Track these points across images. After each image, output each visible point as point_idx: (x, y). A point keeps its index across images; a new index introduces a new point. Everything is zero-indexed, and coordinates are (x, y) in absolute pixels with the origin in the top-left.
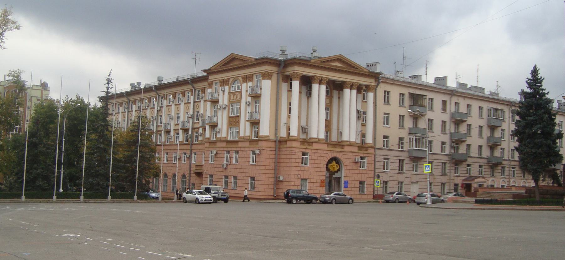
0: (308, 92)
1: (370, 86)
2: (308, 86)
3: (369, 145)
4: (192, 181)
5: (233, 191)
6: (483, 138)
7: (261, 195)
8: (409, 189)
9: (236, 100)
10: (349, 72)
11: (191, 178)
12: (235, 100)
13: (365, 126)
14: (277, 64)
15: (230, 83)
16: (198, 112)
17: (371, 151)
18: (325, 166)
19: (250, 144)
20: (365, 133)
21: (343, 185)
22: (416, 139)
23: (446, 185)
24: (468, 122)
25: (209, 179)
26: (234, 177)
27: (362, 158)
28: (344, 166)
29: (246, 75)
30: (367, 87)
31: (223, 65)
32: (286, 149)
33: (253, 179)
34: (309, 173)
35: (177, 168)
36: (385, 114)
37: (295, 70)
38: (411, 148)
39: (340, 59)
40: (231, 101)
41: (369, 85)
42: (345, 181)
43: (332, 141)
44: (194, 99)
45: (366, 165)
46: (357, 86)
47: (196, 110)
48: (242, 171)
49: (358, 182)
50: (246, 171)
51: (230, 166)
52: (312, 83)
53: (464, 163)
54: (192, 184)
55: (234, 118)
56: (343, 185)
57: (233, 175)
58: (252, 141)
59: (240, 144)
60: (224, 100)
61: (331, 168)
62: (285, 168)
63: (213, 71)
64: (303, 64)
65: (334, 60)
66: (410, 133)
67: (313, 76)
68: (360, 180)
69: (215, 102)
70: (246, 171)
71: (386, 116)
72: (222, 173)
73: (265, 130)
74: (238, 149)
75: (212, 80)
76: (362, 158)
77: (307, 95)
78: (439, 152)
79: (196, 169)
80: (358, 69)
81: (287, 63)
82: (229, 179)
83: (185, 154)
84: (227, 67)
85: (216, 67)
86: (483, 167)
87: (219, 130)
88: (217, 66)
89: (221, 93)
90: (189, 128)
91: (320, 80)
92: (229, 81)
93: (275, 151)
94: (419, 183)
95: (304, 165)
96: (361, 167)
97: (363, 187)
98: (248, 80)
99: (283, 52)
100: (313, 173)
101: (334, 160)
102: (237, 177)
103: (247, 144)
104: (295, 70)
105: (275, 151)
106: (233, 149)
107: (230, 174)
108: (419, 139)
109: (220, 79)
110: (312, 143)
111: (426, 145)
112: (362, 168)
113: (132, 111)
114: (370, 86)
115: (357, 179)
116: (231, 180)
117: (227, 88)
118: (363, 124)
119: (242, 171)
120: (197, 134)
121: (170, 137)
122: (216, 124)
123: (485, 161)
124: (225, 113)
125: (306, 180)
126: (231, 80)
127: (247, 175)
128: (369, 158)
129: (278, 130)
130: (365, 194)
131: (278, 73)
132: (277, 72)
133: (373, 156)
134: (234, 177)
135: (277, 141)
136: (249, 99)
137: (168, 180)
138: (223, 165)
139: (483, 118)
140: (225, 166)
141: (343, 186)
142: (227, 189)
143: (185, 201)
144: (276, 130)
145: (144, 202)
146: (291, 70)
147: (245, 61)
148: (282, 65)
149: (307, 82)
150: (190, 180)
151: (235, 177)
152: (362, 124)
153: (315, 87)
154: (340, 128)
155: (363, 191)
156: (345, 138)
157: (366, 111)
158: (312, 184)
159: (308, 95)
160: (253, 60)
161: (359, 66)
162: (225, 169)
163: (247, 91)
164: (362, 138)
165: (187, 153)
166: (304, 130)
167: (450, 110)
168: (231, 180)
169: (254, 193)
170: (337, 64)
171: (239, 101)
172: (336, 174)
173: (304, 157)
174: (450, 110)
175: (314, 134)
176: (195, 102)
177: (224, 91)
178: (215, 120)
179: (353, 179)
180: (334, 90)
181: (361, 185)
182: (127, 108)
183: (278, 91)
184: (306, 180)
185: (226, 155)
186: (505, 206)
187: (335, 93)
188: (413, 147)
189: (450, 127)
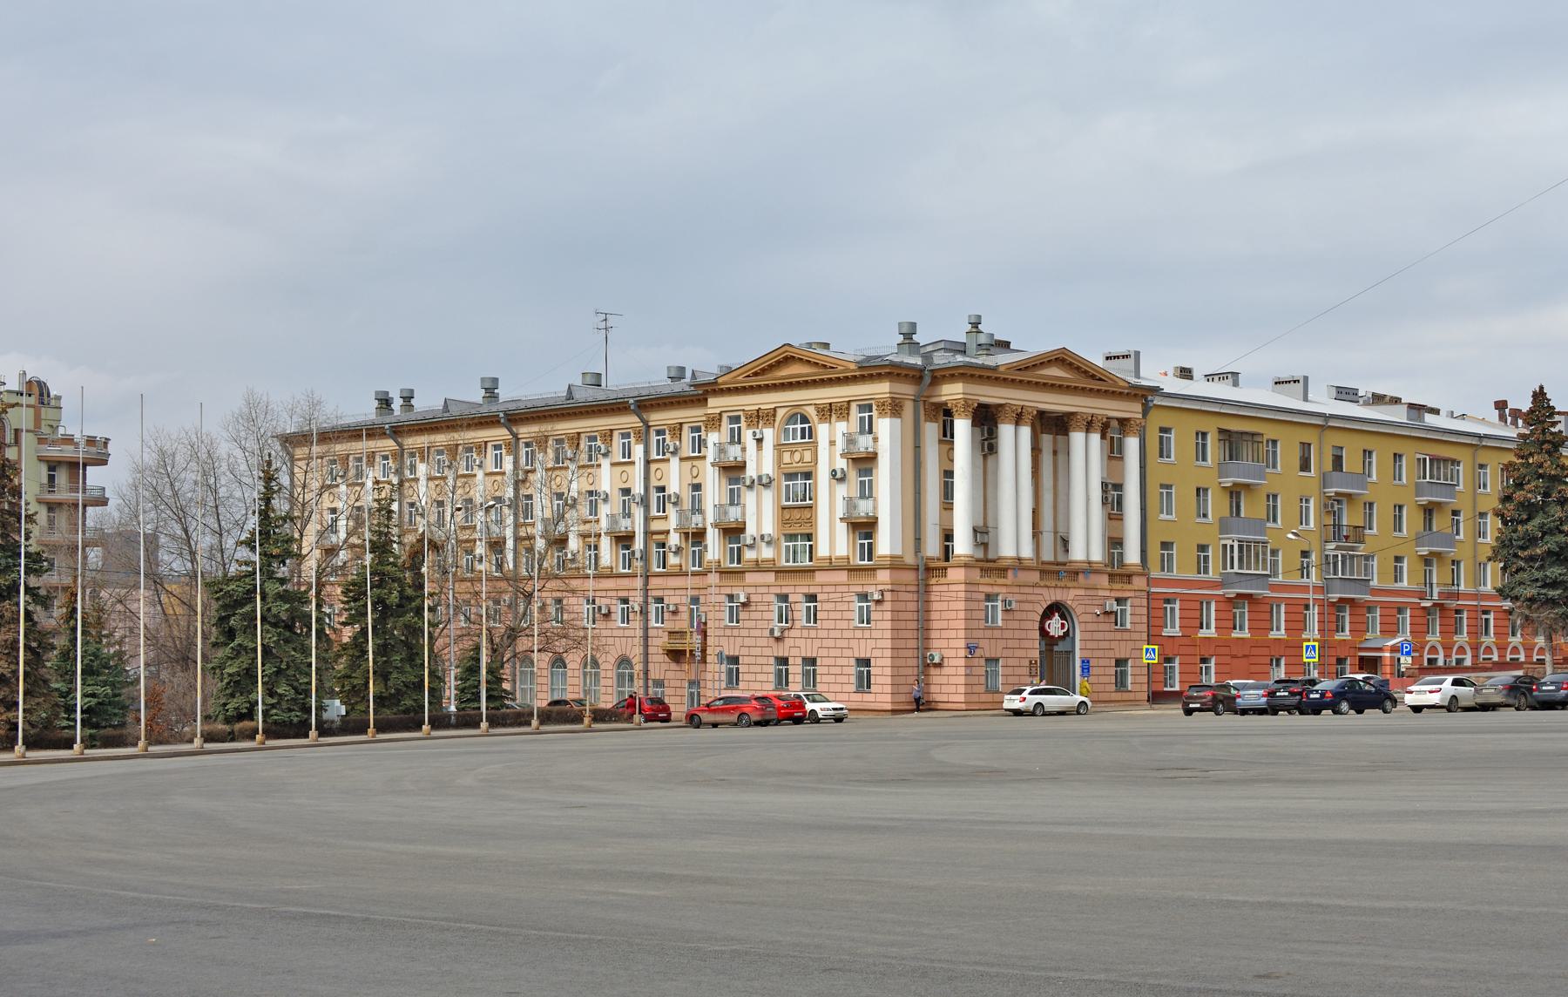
0: (986, 443)
1: (1132, 422)
2: (986, 428)
3: (1133, 569)
4: (654, 674)
8: (1218, 671)
10: (1083, 389)
11: (651, 666)
12: (798, 465)
13: (1122, 520)
14: (913, 376)
15: (778, 419)
16: (662, 489)
17: (1139, 582)
18: (1037, 626)
20: (1122, 539)
22: (1240, 547)
26: (777, 658)
27: (1119, 601)
28: (1080, 623)
29: (830, 404)
30: (1123, 422)
31: (756, 374)
32: (945, 588)
36: (1162, 486)
38: (1229, 570)
39: (1062, 358)
40: (782, 466)
41: (1127, 420)
42: (1083, 662)
43: (1043, 563)
44: (647, 452)
45: (1128, 618)
46: (1102, 424)
47: (654, 483)
49: (1113, 663)
51: (793, 633)
52: (999, 421)
54: (654, 680)
55: (796, 510)
57: (776, 655)
58: (853, 570)
59: (820, 577)
60: (761, 461)
62: (945, 634)
63: (722, 387)
64: (980, 377)
65: (1049, 361)
67: (1001, 405)
68: (1118, 656)
69: (733, 471)
70: (844, 643)
71: (1164, 491)
72: (767, 652)
73: (963, 545)
74: (812, 590)
75: (718, 411)
76: (1119, 601)
77: (983, 450)
79: (671, 641)
81: (938, 374)
82: (739, 666)
83: (625, 601)
85: (735, 377)
87: (752, 542)
88: (739, 376)
89: (751, 444)
90: (634, 532)
91: (1017, 414)
92: (774, 415)
96: (1116, 625)
97: (1124, 674)
98: (834, 417)
99: (908, 334)
100: (826, 643)
101: (1055, 609)
103: (842, 576)
106: (799, 589)
107: (794, 652)
108: (1249, 547)
111: (1264, 560)
112: (1118, 627)
113: (416, 480)
114: (1132, 422)
115: (1111, 654)
116: (796, 669)
117: (769, 434)
118: (1112, 517)
120: (413, 508)
121: (569, 556)
122: (743, 526)
125: (997, 660)
126: (781, 413)
127: (847, 653)
128: (1137, 602)
129: (922, 540)
130: (1130, 691)
131: (914, 400)
132: (913, 398)
133: (1145, 593)
134: (777, 658)
136: (841, 464)
137: (568, 675)
138: (772, 631)
140: (777, 634)
143: (814, 718)
144: (918, 541)
147: (825, 366)
148: (927, 380)
149: (986, 419)
150: (646, 672)
151: (812, 661)
152: (1109, 514)
153: (1006, 431)
154: (1061, 529)
156: (1077, 553)
157: (1121, 482)
158: (1010, 671)
159: (986, 450)
160: (853, 367)
161: (1105, 372)
162: (778, 639)
163: (832, 443)
164: (1112, 551)
165: (630, 599)
168: (796, 669)
169: (867, 697)
170: (1055, 372)
172: (1060, 643)
173: (990, 604)
175: (1007, 549)
176: (648, 462)
177: (759, 441)
178: (734, 514)
179: (1100, 654)
180: (1042, 433)
181: (1119, 669)
182: (397, 470)
184: (997, 660)
186: (883, 790)
187: (1047, 440)
188: (1232, 567)
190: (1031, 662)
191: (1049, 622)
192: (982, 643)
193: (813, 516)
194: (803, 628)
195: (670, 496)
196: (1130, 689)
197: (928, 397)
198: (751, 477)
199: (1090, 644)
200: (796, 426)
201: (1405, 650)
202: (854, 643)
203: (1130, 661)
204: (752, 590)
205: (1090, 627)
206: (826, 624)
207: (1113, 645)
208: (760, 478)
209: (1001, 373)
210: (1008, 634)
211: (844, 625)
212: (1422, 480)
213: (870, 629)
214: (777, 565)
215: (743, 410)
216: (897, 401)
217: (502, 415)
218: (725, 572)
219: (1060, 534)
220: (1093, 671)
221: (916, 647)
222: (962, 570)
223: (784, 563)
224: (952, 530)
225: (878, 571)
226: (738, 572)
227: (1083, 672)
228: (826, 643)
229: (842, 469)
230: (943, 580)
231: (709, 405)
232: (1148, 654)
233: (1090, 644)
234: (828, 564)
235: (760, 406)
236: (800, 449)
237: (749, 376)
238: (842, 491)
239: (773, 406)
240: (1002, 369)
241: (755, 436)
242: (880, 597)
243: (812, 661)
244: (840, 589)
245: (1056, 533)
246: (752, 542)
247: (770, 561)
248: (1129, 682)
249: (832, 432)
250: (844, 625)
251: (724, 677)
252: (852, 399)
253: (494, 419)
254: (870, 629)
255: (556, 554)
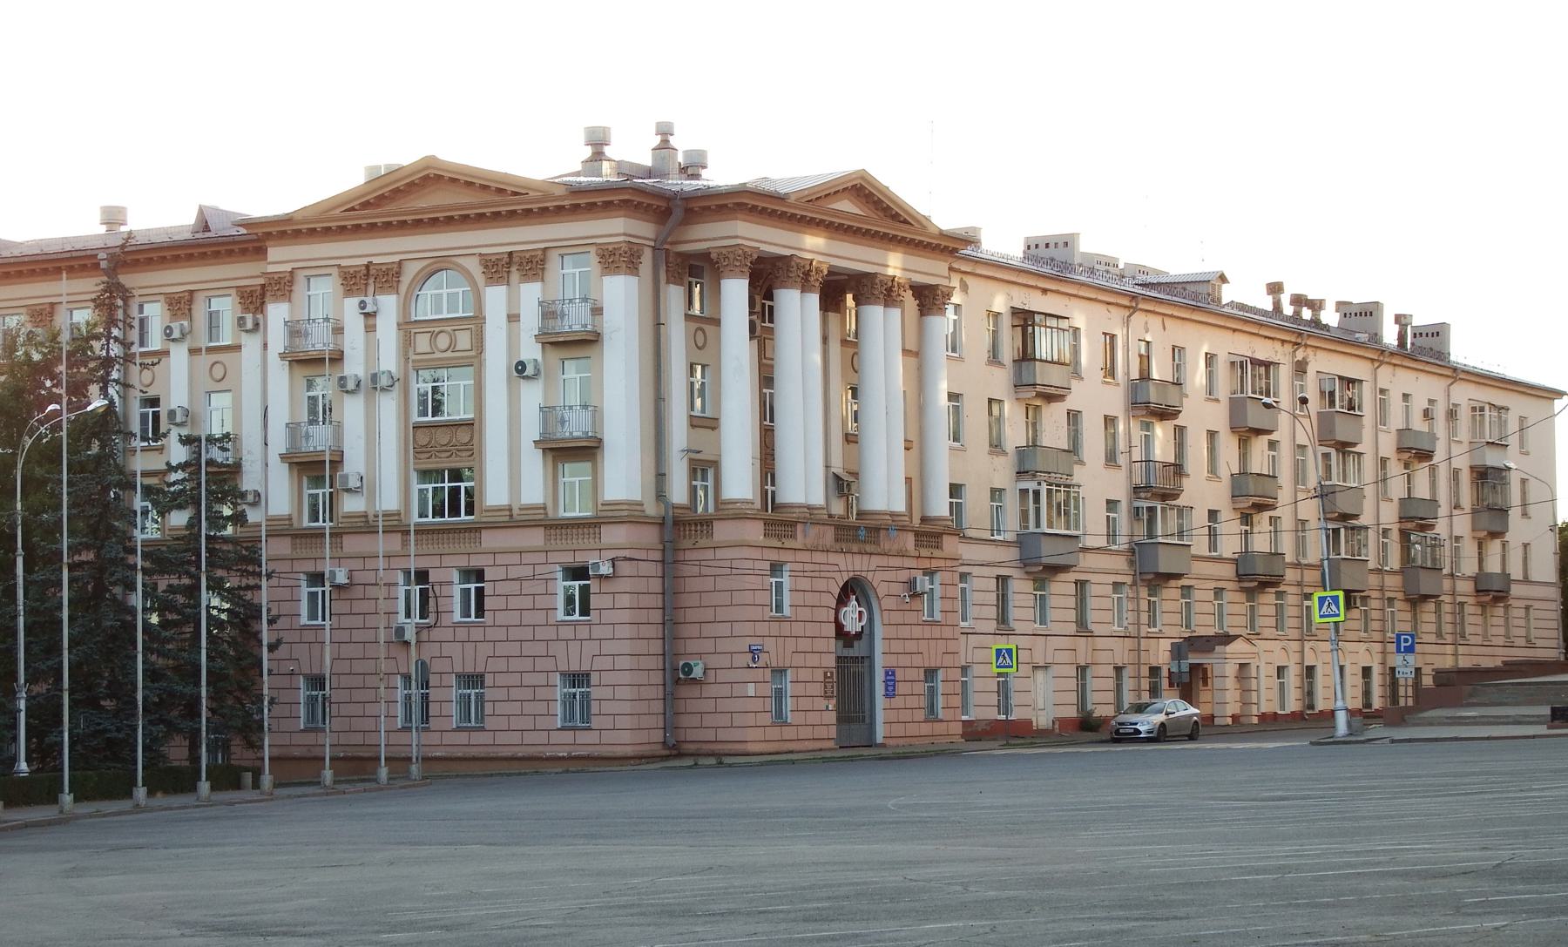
5: (462, 738)
6: (1004, 453)
7: (623, 740)
9: (449, 354)
19: (547, 538)
21: (880, 688)
23: (1125, 673)
24: (1071, 402)
25: (399, 695)
29: (510, 254)
32: (709, 554)
33: (578, 679)
34: (485, 650)
35: (328, 649)
37: (736, 237)
42: (887, 674)
48: (804, 644)
50: (911, 646)
51: (436, 634)
53: (1062, 576)
56: (880, 688)
59: (490, 540)
61: (844, 623)
65: (836, 193)
66: (1021, 473)
73: (739, 483)
74: (476, 562)
75: (287, 267)
78: (1101, 542)
80: (911, 224)
81: (696, 205)
84: (390, 213)
86: (1227, 596)
87: (359, 484)
92: (398, 274)
93: (663, 562)
94: (1055, 670)
95: (576, 617)
100: (502, 649)
102: (588, 675)
103: (536, 538)
104: (736, 237)
105: (663, 562)
106: (447, 561)
109: (344, 263)
110: (939, 535)
115: (917, 660)
117: (388, 305)
119: (804, 644)
123: (1228, 571)
124: (388, 406)
126: (411, 270)
135: (669, 522)
139: (1217, 400)
141: (883, 692)
142: (589, 729)
144: (661, 477)
145: (314, 795)
146: (709, 235)
148: (678, 213)
155: (586, 715)
166: (843, 485)
167: (1128, 374)
169: (583, 737)
171: (467, 357)
174: (1128, 374)
178: (319, 440)
180: (668, 282)
183: (912, 360)
185: (561, 585)
188: (1038, 525)
189: (1228, 448)
190: (825, 673)
191: (845, 609)
192: (769, 644)
193: (475, 441)
194: (456, 625)
195: (172, 414)
196: (940, 717)
197: (673, 243)
198: (356, 376)
199: (897, 646)
200: (440, 291)
201: (1403, 644)
202: (558, 649)
203: (789, 672)
204: (357, 564)
205: (897, 617)
206: (502, 618)
207: (923, 645)
208: (374, 378)
209: (790, 206)
210: (798, 629)
211: (539, 617)
212: (1239, 395)
213: (589, 624)
214: (551, 514)
215: (339, 266)
216: (635, 248)
217: (102, 255)
218: (556, 526)
219: (833, 470)
220: (902, 688)
221: (661, 653)
222: (288, 540)
223: (306, 523)
224: (720, 455)
225: (604, 528)
226: (470, 530)
227: (887, 690)
228: (502, 649)
229: (536, 360)
230: (703, 542)
231: (270, 259)
232: (1001, 659)
233: (897, 646)
234: (507, 519)
235: (370, 259)
236: (449, 329)
237: (352, 209)
238: (532, 396)
239: (396, 258)
240: (792, 199)
241: (364, 308)
242: (611, 570)
243: (473, 680)
244: (528, 558)
245: (827, 467)
246: (359, 484)
247: (540, 508)
248: (940, 706)
249: (513, 300)
250: (539, 617)
251: (558, 708)
252: (547, 245)
253: (88, 262)
254: (589, 624)
255: (307, 492)
